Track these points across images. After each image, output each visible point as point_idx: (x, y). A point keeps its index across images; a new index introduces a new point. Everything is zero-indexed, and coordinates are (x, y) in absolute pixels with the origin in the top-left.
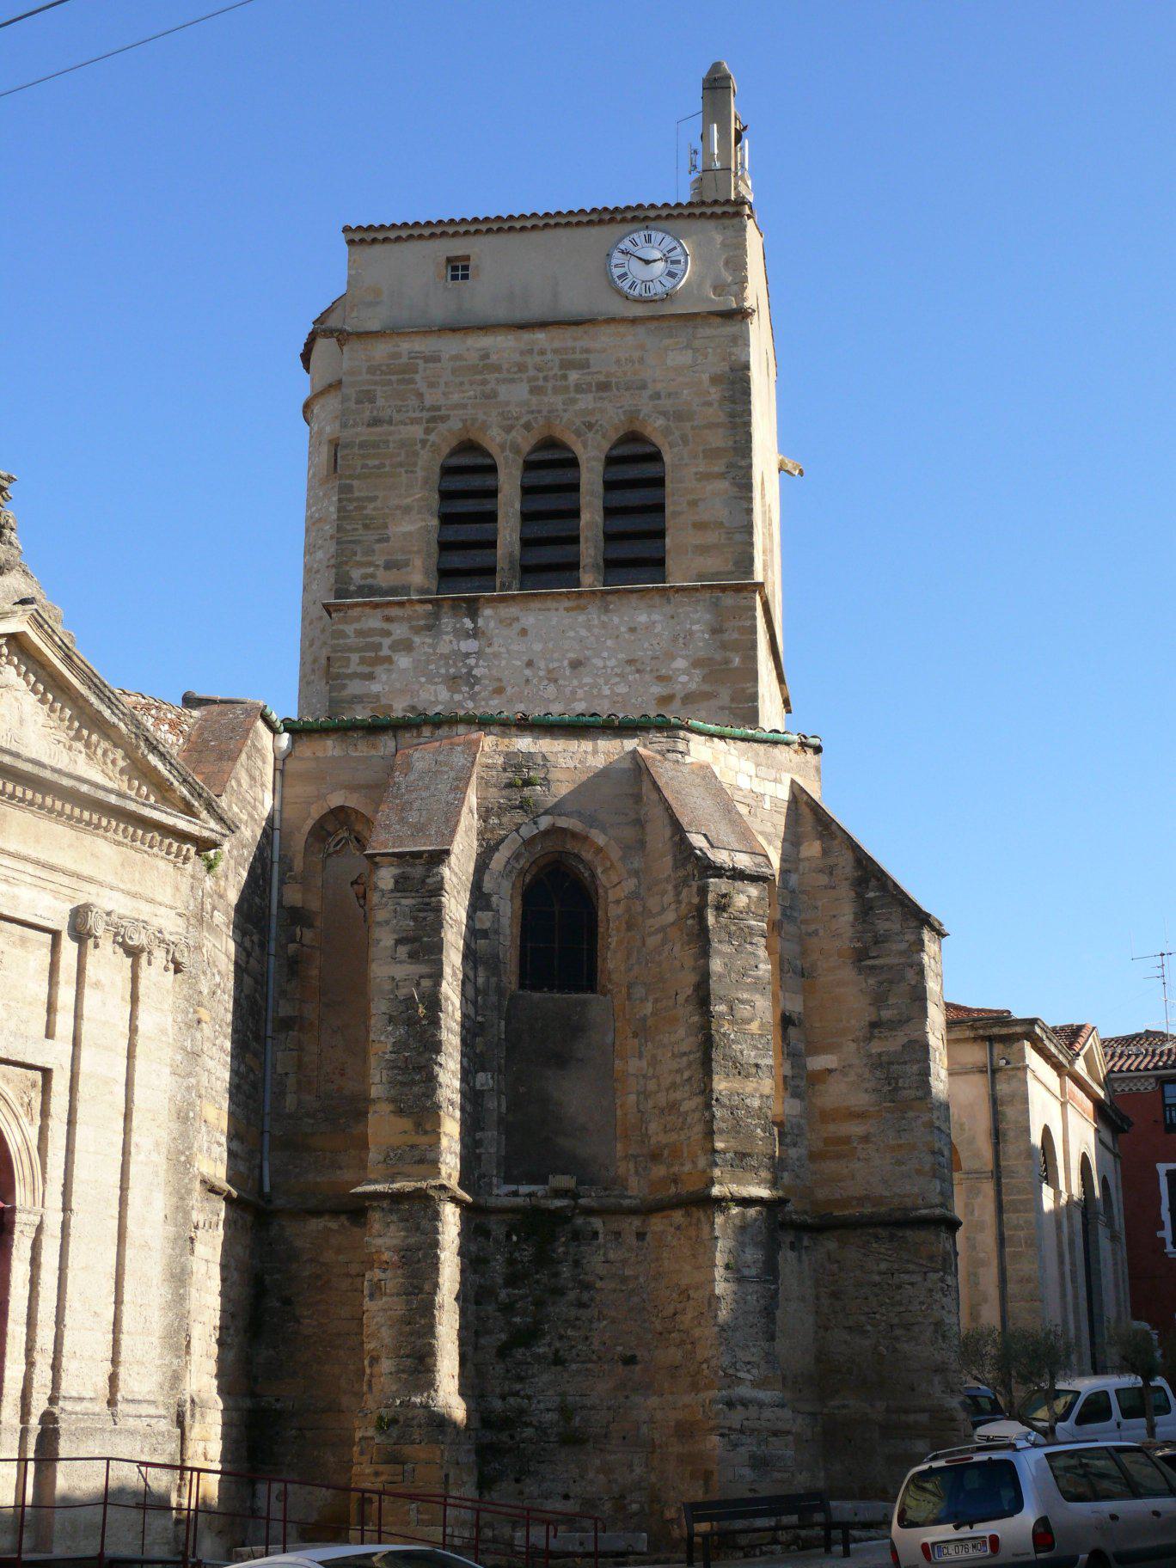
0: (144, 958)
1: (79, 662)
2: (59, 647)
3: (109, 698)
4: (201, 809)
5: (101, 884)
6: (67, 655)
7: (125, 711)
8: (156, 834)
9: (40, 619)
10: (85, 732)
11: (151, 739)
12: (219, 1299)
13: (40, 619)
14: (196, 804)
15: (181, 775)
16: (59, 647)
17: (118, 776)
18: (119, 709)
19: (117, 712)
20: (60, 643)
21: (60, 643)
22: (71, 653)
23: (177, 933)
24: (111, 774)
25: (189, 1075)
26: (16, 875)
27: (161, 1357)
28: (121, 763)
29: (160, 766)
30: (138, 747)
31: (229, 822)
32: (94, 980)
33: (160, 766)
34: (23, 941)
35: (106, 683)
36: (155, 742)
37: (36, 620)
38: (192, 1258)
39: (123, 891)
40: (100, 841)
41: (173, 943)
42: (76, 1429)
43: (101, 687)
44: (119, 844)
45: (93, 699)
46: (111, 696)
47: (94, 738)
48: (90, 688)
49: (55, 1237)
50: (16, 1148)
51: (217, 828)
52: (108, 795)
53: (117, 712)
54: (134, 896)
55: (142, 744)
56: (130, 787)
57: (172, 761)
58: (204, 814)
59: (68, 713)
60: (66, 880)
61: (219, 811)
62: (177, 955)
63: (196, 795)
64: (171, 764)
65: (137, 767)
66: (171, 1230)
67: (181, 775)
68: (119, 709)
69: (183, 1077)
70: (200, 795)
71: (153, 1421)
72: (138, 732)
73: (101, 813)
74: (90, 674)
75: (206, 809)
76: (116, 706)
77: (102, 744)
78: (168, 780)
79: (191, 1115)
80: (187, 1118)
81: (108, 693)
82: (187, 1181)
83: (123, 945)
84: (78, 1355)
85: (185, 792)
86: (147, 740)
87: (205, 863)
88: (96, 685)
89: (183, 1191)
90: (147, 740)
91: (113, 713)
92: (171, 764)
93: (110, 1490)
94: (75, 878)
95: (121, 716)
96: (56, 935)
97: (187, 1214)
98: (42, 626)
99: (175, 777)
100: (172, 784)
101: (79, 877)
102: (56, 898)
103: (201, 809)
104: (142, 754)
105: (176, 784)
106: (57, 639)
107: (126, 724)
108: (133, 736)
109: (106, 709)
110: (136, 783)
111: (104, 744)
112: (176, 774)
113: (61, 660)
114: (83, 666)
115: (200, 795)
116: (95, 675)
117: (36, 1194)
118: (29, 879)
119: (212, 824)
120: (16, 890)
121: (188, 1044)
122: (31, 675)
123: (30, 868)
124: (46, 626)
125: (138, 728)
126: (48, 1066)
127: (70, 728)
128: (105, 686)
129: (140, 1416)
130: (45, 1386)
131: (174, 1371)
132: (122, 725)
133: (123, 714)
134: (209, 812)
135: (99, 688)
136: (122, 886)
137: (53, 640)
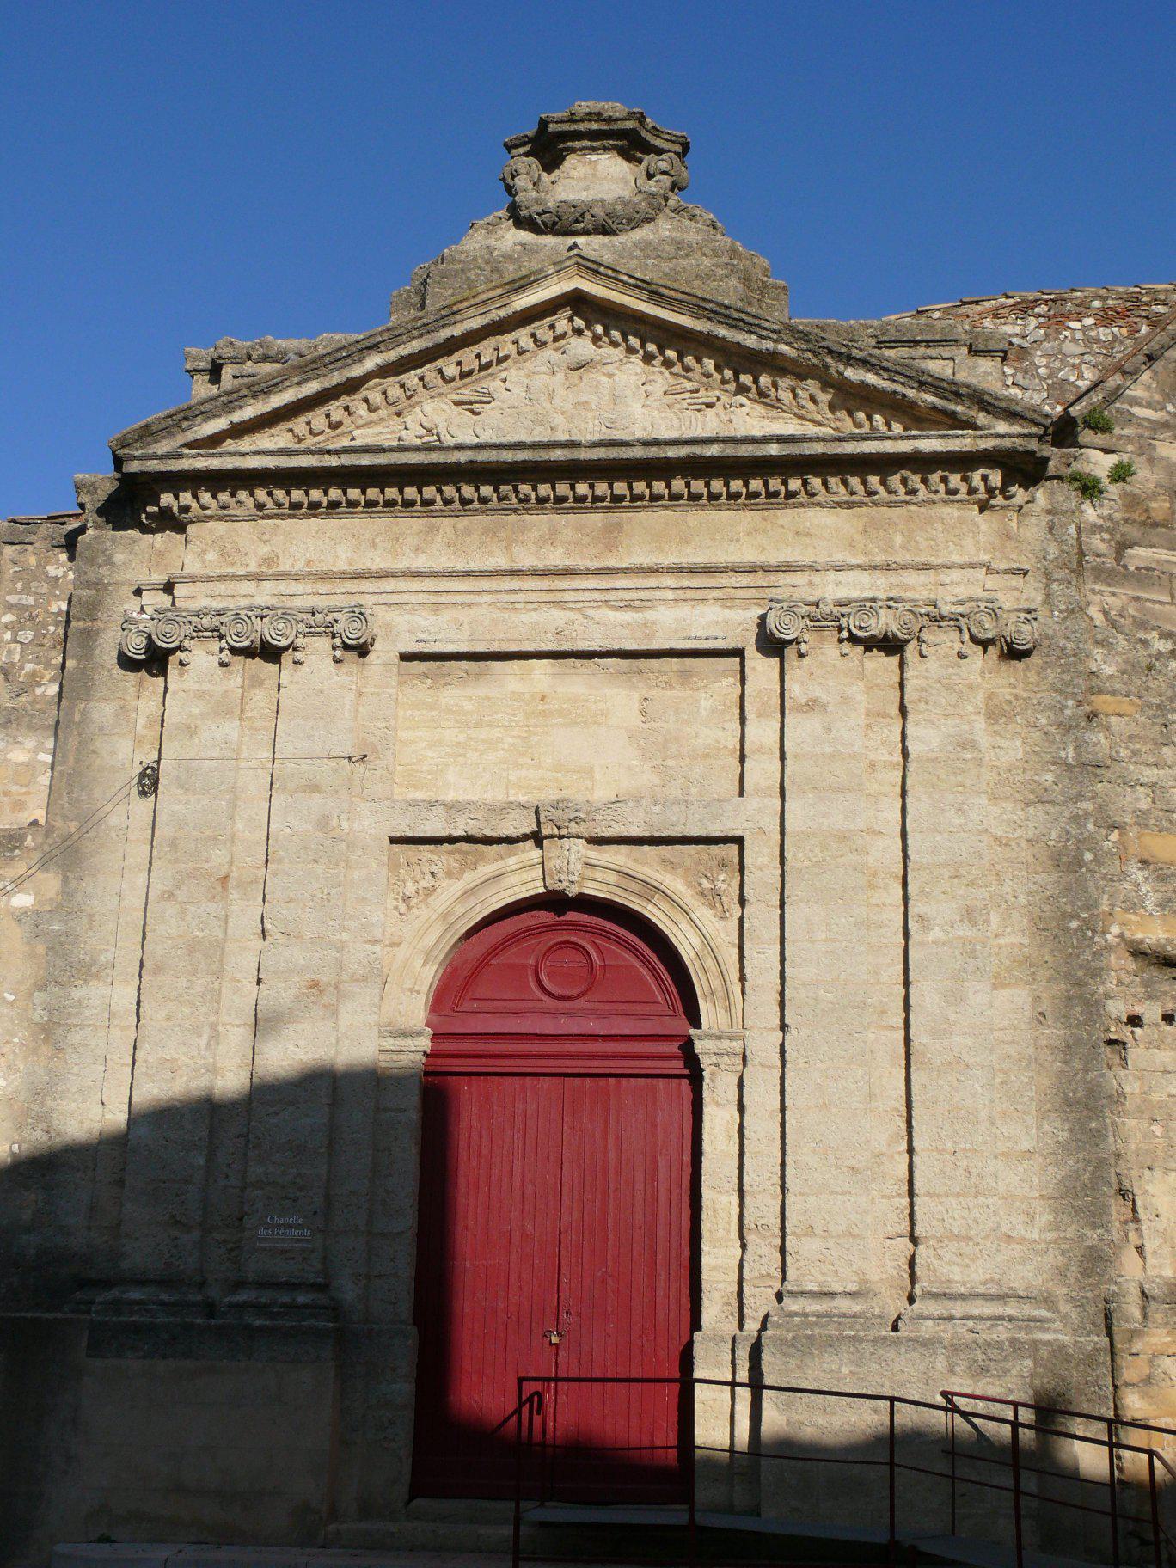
0: (910, 652)
1: (672, 293)
2: (636, 286)
3: (743, 320)
4: (972, 413)
5: (813, 568)
6: (650, 292)
7: (774, 327)
8: (907, 473)
9: (589, 264)
10: (746, 379)
11: (835, 348)
12: (117, 1117)
13: (589, 264)
14: (959, 408)
15: (911, 378)
16: (636, 286)
17: (830, 415)
18: (765, 329)
19: (764, 333)
20: (632, 281)
21: (632, 281)
22: (654, 286)
23: (971, 600)
24: (818, 418)
25: (1078, 798)
26: (642, 595)
27: (1054, 1226)
28: (825, 398)
29: (871, 378)
30: (827, 367)
31: (1027, 414)
32: (803, 700)
33: (871, 378)
34: (684, 676)
35: (727, 302)
36: (844, 350)
37: (587, 268)
38: (1122, 1072)
39: (859, 567)
40: (812, 513)
41: (962, 616)
42: (795, 1338)
43: (722, 311)
44: (849, 505)
45: (723, 332)
46: (743, 316)
47: (765, 380)
48: (709, 319)
49: (770, 1067)
50: (692, 954)
51: (1016, 429)
52: (762, 446)
53: (764, 333)
54: (887, 568)
55: (828, 360)
56: (858, 425)
57: (885, 364)
58: (982, 418)
59: (709, 364)
60: (744, 579)
61: (1003, 404)
62: (974, 630)
63: (952, 397)
64: (886, 370)
65: (847, 393)
66: (1054, 1033)
67: (911, 378)
68: (765, 329)
69: (1064, 804)
70: (958, 395)
71: (979, 1326)
72: (810, 346)
73: (627, 477)
74: (694, 300)
75: (982, 409)
76: (759, 326)
77: (780, 383)
78: (895, 392)
79: (1088, 856)
80: (1078, 862)
81: (737, 315)
82: (1088, 955)
83: (854, 639)
84: (818, 1231)
85: (930, 398)
86: (830, 352)
87: (1076, 485)
88: (715, 312)
89: (1080, 973)
90: (830, 352)
91: (761, 337)
92: (886, 370)
93: (896, 1431)
94: (761, 573)
95: (775, 336)
96: (739, 653)
97: (1093, 1007)
98: (597, 272)
99: (903, 384)
100: (904, 395)
101: (766, 569)
102: (729, 608)
103: (972, 413)
104: (838, 372)
105: (911, 393)
106: (625, 278)
107: (787, 344)
108: (809, 355)
109: (747, 336)
110: (861, 415)
111: (784, 383)
112: (902, 380)
113: (649, 301)
114: (680, 296)
115: (958, 395)
116: (704, 300)
117: (733, 1011)
118: (670, 595)
119: (1002, 427)
120: (649, 615)
121: (1070, 754)
122: (630, 337)
123: (669, 581)
124: (602, 269)
125: (808, 341)
126: (738, 833)
127: (724, 382)
128: (728, 307)
129: (951, 1318)
130: (769, 1276)
131: (1091, 1247)
132: (783, 348)
133: (774, 331)
134: (988, 412)
135: (720, 314)
136: (854, 561)
137: (622, 281)
